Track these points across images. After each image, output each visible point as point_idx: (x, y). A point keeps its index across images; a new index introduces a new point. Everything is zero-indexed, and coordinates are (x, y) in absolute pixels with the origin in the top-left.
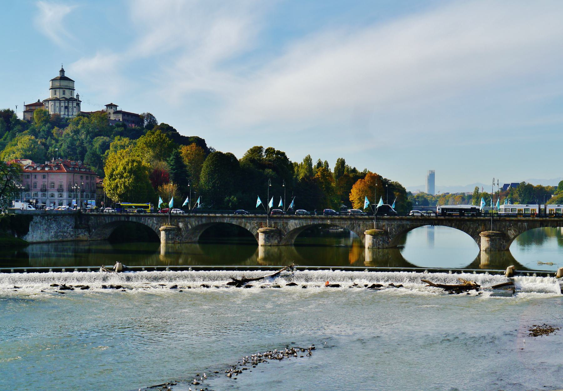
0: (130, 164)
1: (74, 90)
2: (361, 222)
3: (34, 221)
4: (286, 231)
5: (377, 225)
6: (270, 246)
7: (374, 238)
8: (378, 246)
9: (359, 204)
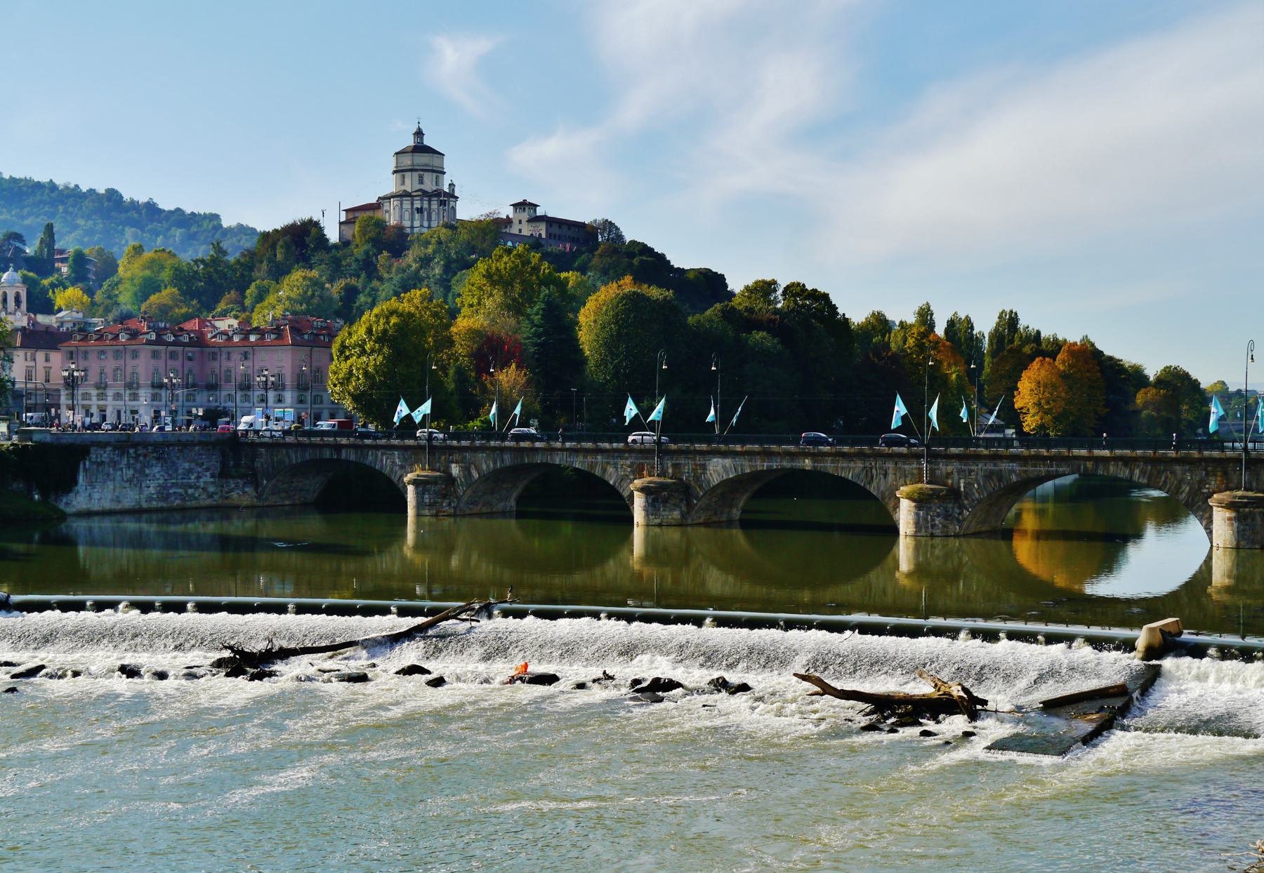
0: (382, 321)
1: (444, 173)
2: (890, 465)
3: (93, 460)
4: (701, 486)
5: (932, 473)
6: (660, 525)
7: (918, 508)
8: (930, 530)
9: (1037, 418)
